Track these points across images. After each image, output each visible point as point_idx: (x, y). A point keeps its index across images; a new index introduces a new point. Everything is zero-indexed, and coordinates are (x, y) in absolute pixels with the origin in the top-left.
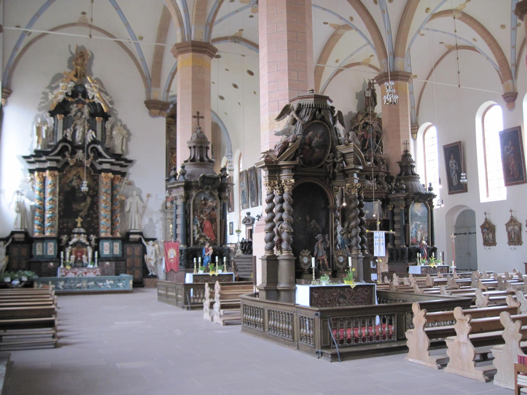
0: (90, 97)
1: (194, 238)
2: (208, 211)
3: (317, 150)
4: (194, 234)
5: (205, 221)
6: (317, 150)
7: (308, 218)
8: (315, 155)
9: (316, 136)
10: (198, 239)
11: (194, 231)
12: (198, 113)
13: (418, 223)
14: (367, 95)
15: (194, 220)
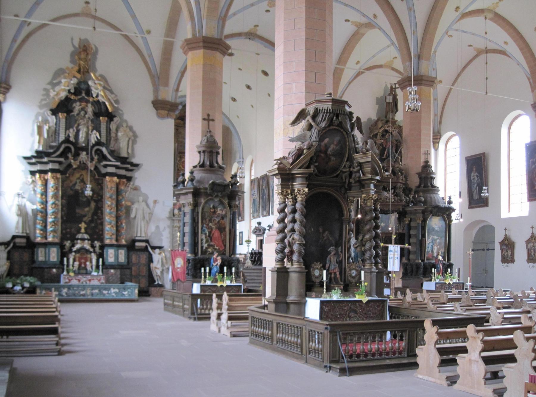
0: (94, 96)
1: (202, 247)
2: (217, 220)
3: (333, 158)
4: (202, 243)
5: (214, 230)
6: (333, 158)
7: (321, 230)
8: (331, 164)
9: (333, 143)
10: (206, 248)
11: (202, 240)
12: (208, 115)
13: (435, 237)
14: (387, 101)
15: (202, 228)
